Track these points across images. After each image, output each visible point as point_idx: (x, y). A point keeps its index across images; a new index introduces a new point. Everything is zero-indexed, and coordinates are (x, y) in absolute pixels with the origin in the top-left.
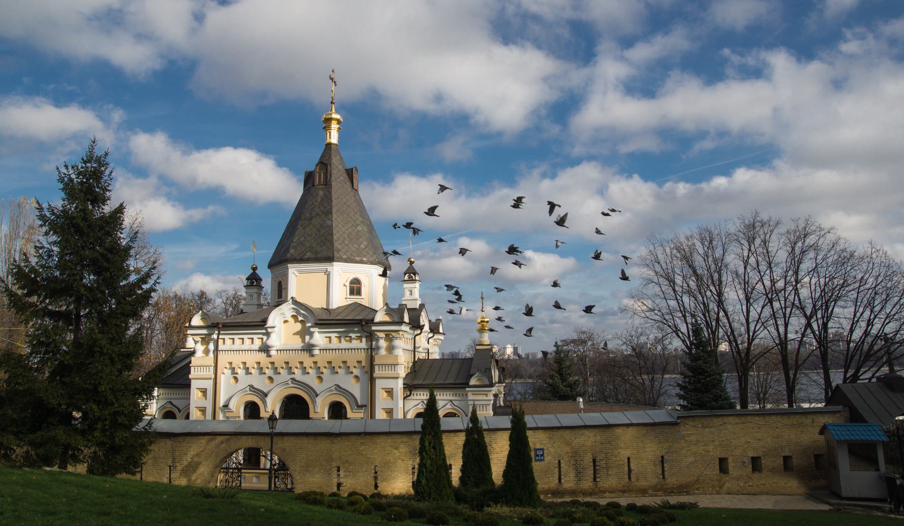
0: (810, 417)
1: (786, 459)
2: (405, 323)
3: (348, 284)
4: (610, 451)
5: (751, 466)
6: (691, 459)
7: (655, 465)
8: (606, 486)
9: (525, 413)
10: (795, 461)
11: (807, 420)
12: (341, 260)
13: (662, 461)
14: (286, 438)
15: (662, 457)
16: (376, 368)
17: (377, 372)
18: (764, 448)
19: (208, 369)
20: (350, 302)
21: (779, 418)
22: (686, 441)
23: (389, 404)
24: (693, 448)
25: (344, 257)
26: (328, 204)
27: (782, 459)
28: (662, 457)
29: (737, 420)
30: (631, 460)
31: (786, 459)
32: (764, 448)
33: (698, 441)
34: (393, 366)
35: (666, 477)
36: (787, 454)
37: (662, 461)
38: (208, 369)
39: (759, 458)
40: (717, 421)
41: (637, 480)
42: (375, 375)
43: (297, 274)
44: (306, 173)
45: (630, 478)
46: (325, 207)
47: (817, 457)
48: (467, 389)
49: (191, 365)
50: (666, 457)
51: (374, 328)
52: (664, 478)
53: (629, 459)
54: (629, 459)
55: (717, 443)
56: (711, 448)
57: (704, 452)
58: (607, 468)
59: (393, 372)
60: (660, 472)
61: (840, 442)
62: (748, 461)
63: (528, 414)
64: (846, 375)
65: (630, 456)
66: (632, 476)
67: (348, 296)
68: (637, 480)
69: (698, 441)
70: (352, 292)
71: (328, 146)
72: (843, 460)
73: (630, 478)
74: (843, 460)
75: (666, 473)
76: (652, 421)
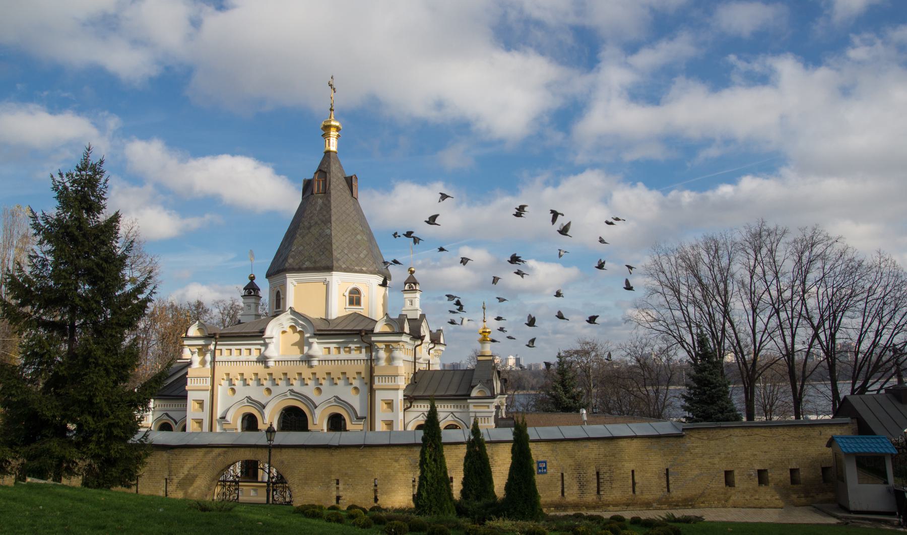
0: (817, 429)
1: (793, 471)
2: (405, 333)
3: (347, 294)
4: (614, 464)
5: (757, 479)
6: (696, 472)
7: (659, 478)
8: (610, 499)
10: (802, 474)
11: (815, 432)
12: (340, 269)
13: (667, 474)
14: (284, 450)
15: (667, 470)
16: (376, 379)
17: (377, 383)
18: (770, 460)
19: (205, 380)
20: (349, 312)
22: (691, 453)
23: (389, 416)
25: (344, 266)
28: (667, 470)
29: (743, 432)
30: (635, 473)
31: (793, 471)
32: (770, 460)
33: (703, 454)
34: (196, 379)
36: (794, 466)
37: (667, 474)
38: (205, 380)
39: (765, 470)
40: (723, 433)
41: (642, 493)
42: (374, 387)
44: (304, 181)
45: (634, 491)
47: (824, 470)
48: (469, 401)
49: (187, 376)
50: (671, 470)
51: (373, 339)
52: (669, 491)
53: (633, 471)
54: (633, 471)
55: (723, 455)
56: (716, 460)
57: (709, 465)
59: (393, 383)
61: (848, 455)
62: (754, 474)
66: (637, 489)
67: (348, 306)
68: (642, 493)
69: (703, 454)
70: (351, 302)
72: (851, 472)
73: (634, 491)
74: (851, 472)
75: (671, 486)
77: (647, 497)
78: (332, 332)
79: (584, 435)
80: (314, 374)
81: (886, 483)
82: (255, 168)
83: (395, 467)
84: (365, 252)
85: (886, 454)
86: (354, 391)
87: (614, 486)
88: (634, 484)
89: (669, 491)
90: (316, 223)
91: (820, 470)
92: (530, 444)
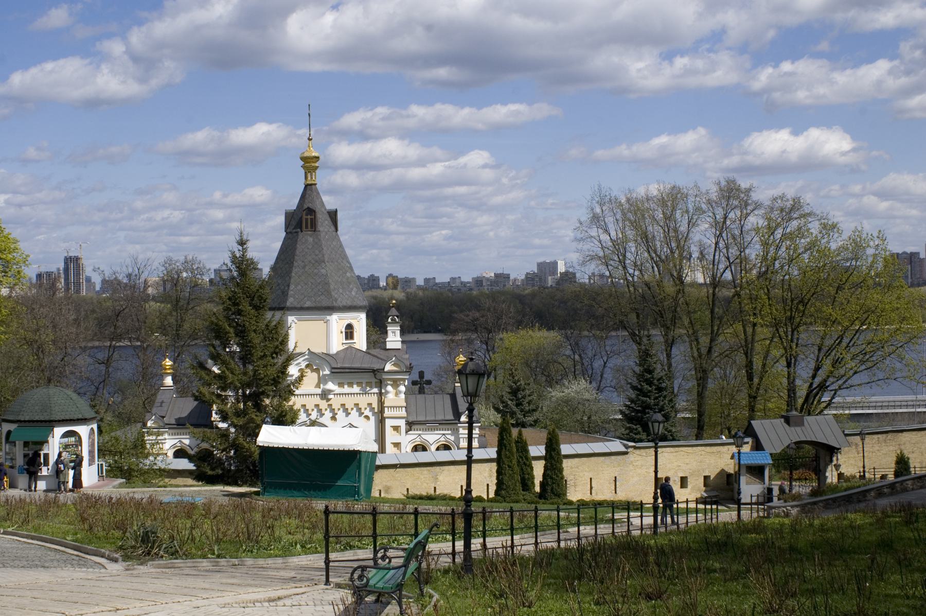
3: (344, 330)
4: (577, 474)
5: (679, 483)
6: (636, 479)
7: (610, 483)
9: (528, 443)
13: (615, 481)
15: (616, 477)
16: (386, 409)
17: (387, 413)
18: (690, 470)
21: (703, 448)
24: (639, 471)
26: (320, 252)
27: (703, 478)
28: (616, 477)
30: (593, 480)
32: (690, 470)
33: (642, 466)
35: (617, 492)
36: (707, 474)
37: (615, 481)
39: (686, 477)
41: (597, 494)
43: (296, 321)
44: (286, 213)
45: (591, 494)
46: (317, 255)
48: (459, 425)
52: (616, 493)
53: (591, 479)
54: (591, 479)
58: (575, 486)
60: (614, 489)
63: (531, 445)
64: (806, 444)
65: (592, 477)
66: (593, 491)
68: (597, 494)
69: (642, 466)
70: (347, 338)
71: (308, 187)
73: (591, 494)
75: (617, 489)
76: (488, 457)
77: (600, 497)
78: (356, 371)
79: (574, 452)
80: (331, 405)
81: (764, 484)
82: (706, 478)
83: (421, 479)
84: (355, 289)
85: (766, 464)
86: (365, 420)
87: (577, 489)
88: (591, 488)
89: (616, 493)
90: (310, 262)
91: (726, 477)
92: (565, 461)
